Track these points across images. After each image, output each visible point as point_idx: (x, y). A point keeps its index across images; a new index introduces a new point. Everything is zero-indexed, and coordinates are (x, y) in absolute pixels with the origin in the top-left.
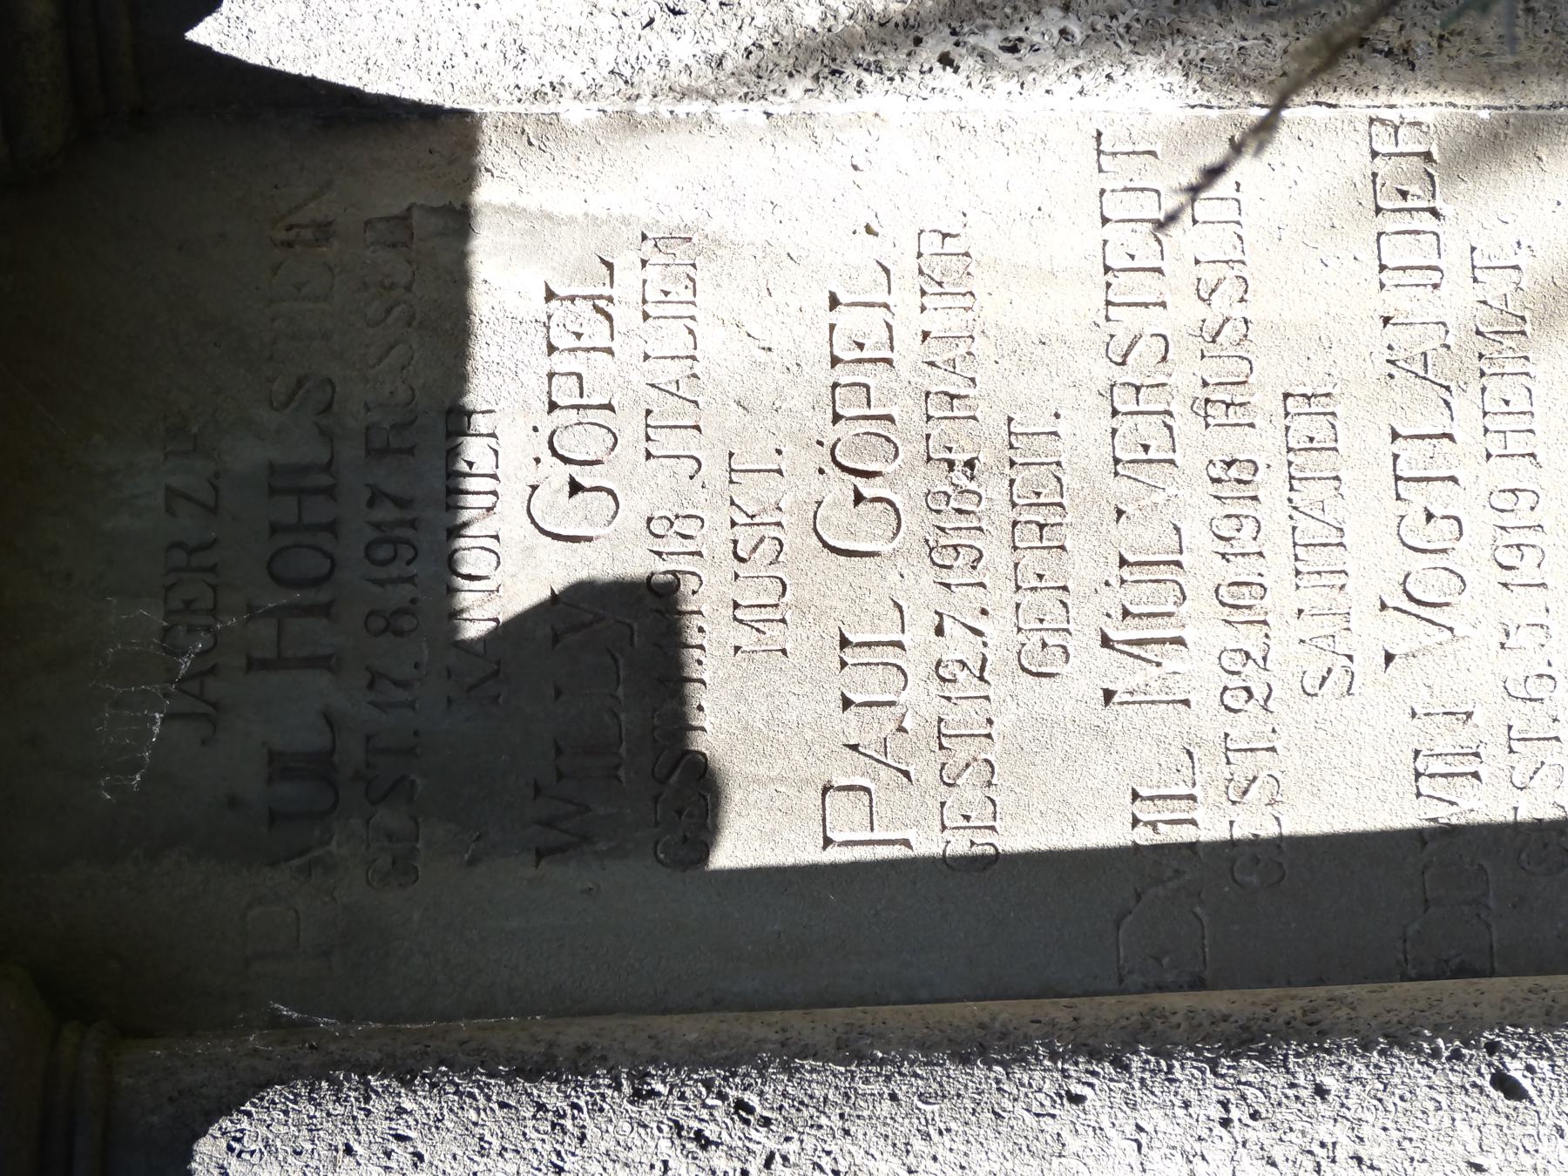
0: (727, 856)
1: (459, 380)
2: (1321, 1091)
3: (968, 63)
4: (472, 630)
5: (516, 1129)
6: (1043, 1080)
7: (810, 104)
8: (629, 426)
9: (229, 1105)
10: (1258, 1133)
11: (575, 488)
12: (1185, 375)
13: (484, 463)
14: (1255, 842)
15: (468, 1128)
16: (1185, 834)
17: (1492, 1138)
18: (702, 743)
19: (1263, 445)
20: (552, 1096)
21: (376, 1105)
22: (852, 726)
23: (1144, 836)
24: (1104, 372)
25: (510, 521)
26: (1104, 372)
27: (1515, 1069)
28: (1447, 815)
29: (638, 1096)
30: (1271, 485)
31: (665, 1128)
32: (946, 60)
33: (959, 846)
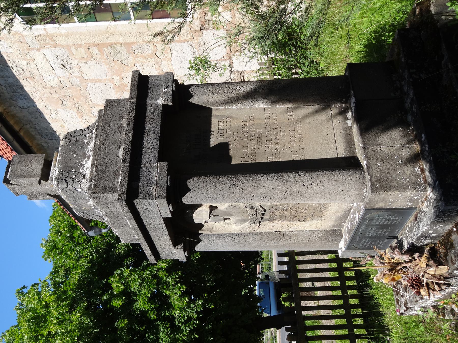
0: (232, 163)
1: (210, 128)
2: (283, 176)
3: (253, 102)
4: (211, 146)
5: (214, 179)
6: (259, 175)
7: (240, 107)
8: (225, 131)
9: (190, 178)
10: (278, 179)
11: (220, 135)
12: (272, 126)
13: (213, 134)
14: (278, 161)
15: (210, 179)
16: (272, 161)
17: (298, 179)
18: (230, 154)
19: (278, 131)
20: (218, 177)
21: (203, 178)
22: (244, 153)
23: (268, 161)
24: (265, 126)
25: (215, 138)
26: (265, 126)
27: (300, 174)
28: (295, 159)
29: (225, 177)
30: (279, 134)
31: (251, 36)
32: (251, 102)
33: (253, 162)
